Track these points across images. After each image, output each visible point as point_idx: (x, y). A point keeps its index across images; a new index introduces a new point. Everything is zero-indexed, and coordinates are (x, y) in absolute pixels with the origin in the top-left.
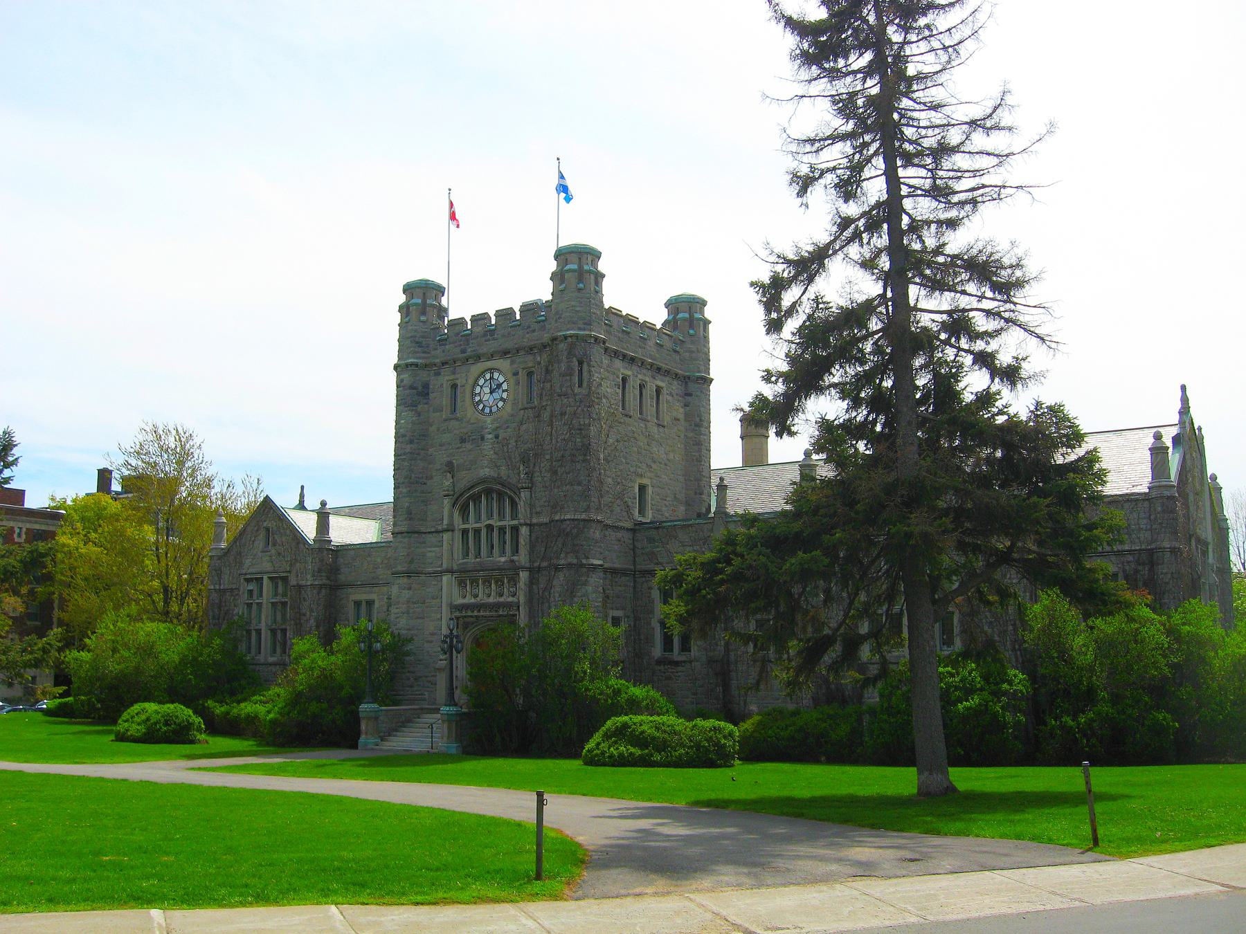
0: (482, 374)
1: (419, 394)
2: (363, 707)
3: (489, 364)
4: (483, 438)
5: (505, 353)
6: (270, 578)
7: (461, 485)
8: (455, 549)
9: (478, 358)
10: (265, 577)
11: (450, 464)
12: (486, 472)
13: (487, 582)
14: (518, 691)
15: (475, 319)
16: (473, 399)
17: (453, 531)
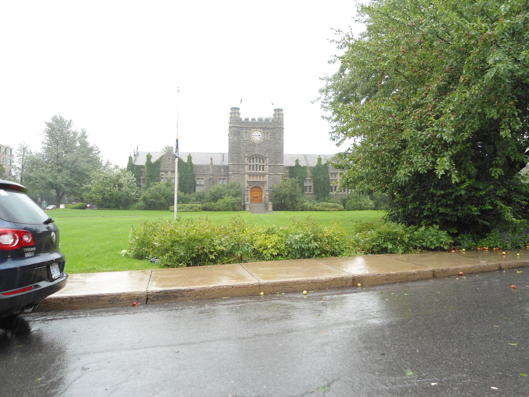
7: (250, 155)
12: (257, 153)
15: (252, 119)
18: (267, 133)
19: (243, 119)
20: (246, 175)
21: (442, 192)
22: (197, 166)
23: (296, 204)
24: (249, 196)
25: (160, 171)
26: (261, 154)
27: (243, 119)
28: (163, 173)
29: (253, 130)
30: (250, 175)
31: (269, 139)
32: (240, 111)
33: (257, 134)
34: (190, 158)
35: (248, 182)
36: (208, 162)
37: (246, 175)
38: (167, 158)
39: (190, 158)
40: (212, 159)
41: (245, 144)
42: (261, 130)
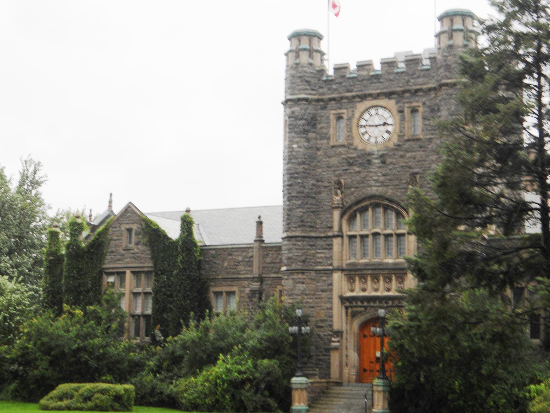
0: (367, 110)
1: (309, 124)
2: (294, 380)
3: (375, 102)
4: (369, 162)
5: (389, 95)
6: (133, 272)
7: (350, 200)
8: (344, 253)
9: (363, 97)
10: (128, 272)
11: (339, 183)
12: (375, 190)
13: (375, 278)
14: (388, 316)
15: (361, 67)
16: (359, 120)
17: (342, 236)
18: (414, 111)
19: (331, 72)
20: (336, 276)
21: (9, 337)
22: (205, 250)
23: (489, 392)
24: (354, 356)
25: (102, 273)
26: (390, 192)
27: (331, 72)
28: (111, 279)
29: (361, 106)
30: (353, 273)
31: (419, 133)
32: (323, 46)
33: (377, 120)
34: (187, 224)
35: (343, 299)
36: (247, 237)
37: (336, 276)
38: (123, 227)
39: (187, 224)
40: (260, 224)
41: (334, 161)
42: (391, 103)
